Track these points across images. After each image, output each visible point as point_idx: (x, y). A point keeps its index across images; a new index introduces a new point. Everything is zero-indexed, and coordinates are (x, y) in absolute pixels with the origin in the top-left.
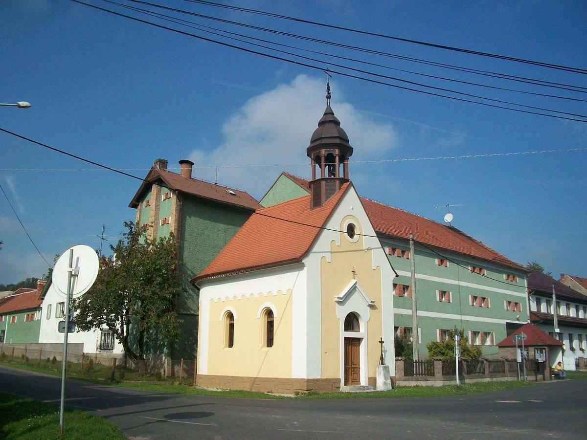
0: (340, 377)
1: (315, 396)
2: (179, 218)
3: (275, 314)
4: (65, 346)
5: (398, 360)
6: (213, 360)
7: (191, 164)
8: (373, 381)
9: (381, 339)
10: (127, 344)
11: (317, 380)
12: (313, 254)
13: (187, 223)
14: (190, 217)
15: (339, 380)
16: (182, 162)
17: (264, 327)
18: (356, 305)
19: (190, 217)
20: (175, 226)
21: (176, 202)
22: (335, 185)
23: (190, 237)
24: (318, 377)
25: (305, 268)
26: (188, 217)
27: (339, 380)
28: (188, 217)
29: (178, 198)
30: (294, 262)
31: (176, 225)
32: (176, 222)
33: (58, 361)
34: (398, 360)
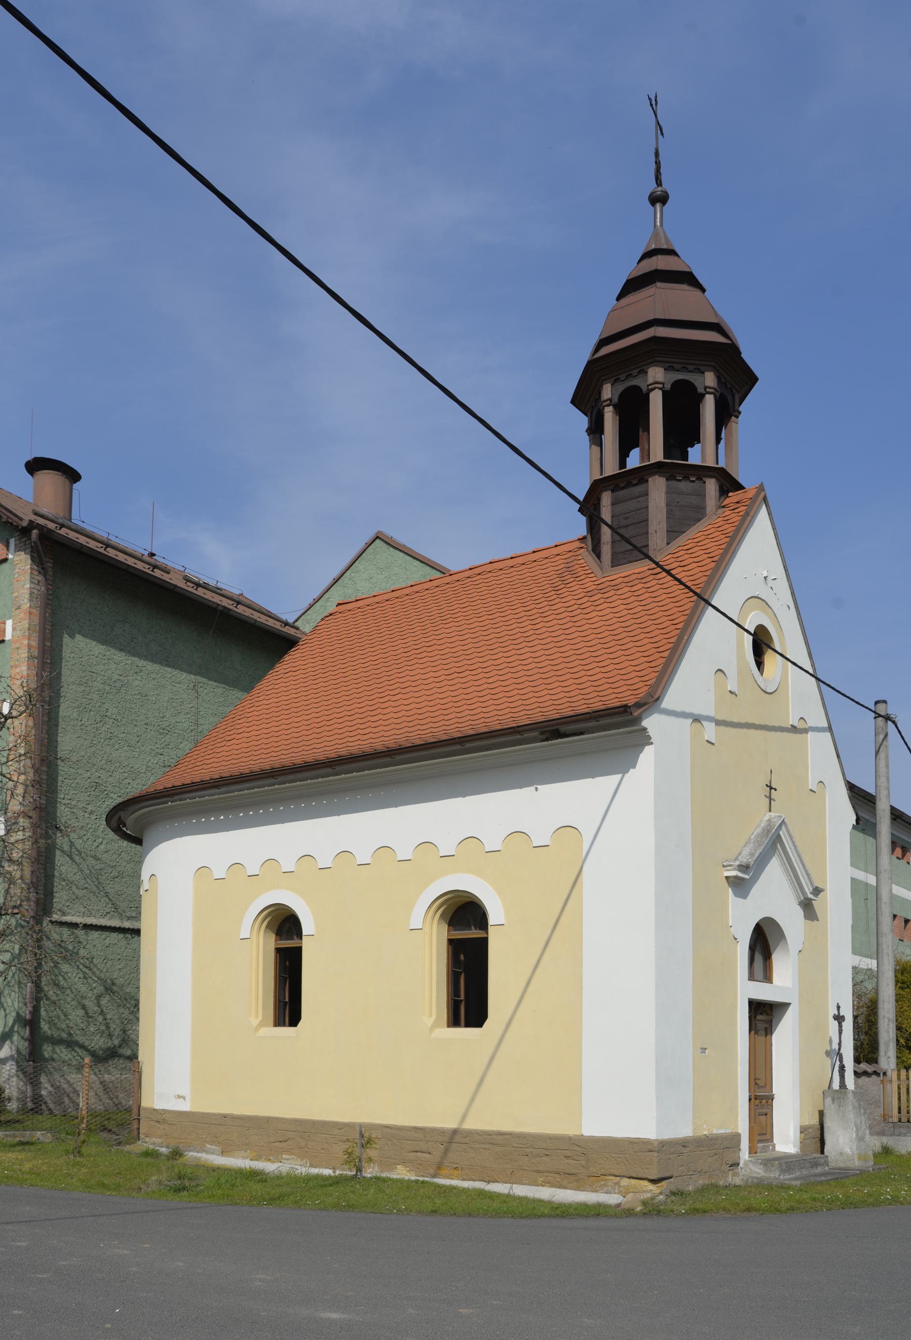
0: (740, 1131)
1: (688, 1193)
2: (44, 621)
3: (308, 926)
4: (127, 924)
5: (865, 1073)
6: (197, 1047)
7: (73, 476)
8: (816, 1136)
9: (838, 1007)
10: (161, 1154)
11: (684, 1143)
12: (663, 717)
13: (66, 652)
14: (72, 636)
15: (735, 1138)
16: (35, 466)
17: (438, 959)
18: (772, 897)
19: (72, 636)
20: (29, 647)
21: (32, 569)
22: (702, 495)
23: (81, 689)
24: (684, 1130)
25: (647, 755)
26: (66, 636)
27: (737, 1137)
28: (66, 636)
29: (38, 560)
30: (595, 729)
31: (34, 644)
32: (35, 636)
33: (138, 863)
34: (865, 1073)
